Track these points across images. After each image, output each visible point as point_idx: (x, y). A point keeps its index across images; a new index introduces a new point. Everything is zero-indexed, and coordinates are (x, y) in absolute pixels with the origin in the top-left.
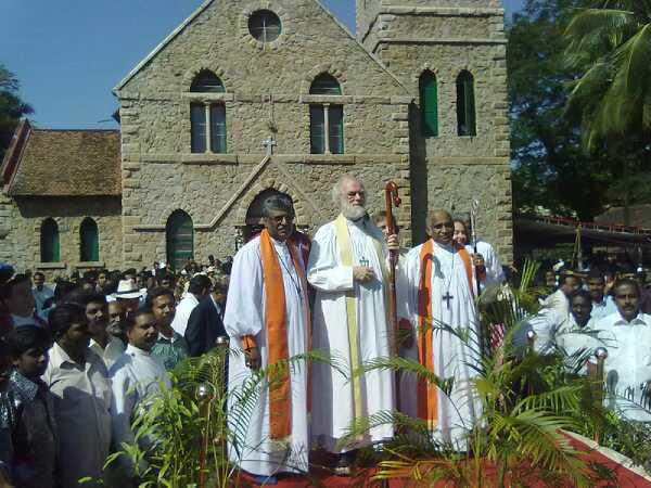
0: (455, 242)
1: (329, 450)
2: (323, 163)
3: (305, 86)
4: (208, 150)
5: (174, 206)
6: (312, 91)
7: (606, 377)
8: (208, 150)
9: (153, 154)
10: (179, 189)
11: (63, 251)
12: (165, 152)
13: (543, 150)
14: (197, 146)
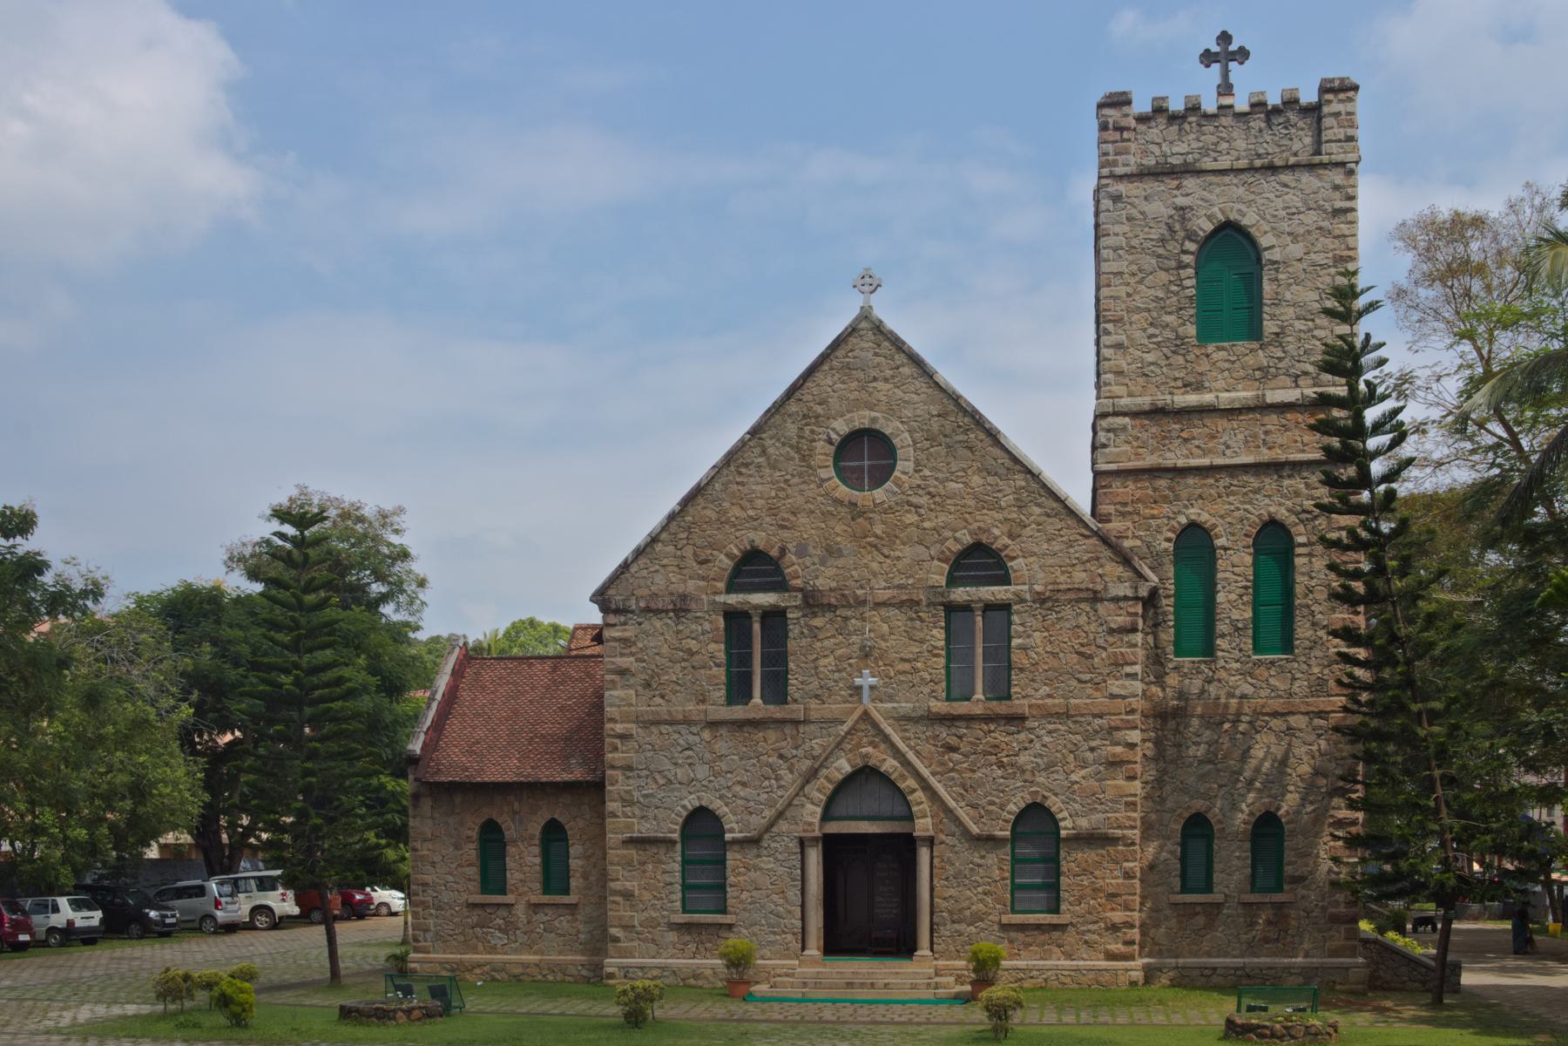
0: (193, 744)
1: (1223, 1028)
2: (969, 719)
3: (938, 575)
4: (757, 699)
5: (691, 802)
6: (952, 581)
7: (1394, 422)
8: (757, 699)
9: (661, 708)
10: (702, 772)
11: (513, 877)
12: (685, 706)
13: (1350, 422)
14: (739, 690)
